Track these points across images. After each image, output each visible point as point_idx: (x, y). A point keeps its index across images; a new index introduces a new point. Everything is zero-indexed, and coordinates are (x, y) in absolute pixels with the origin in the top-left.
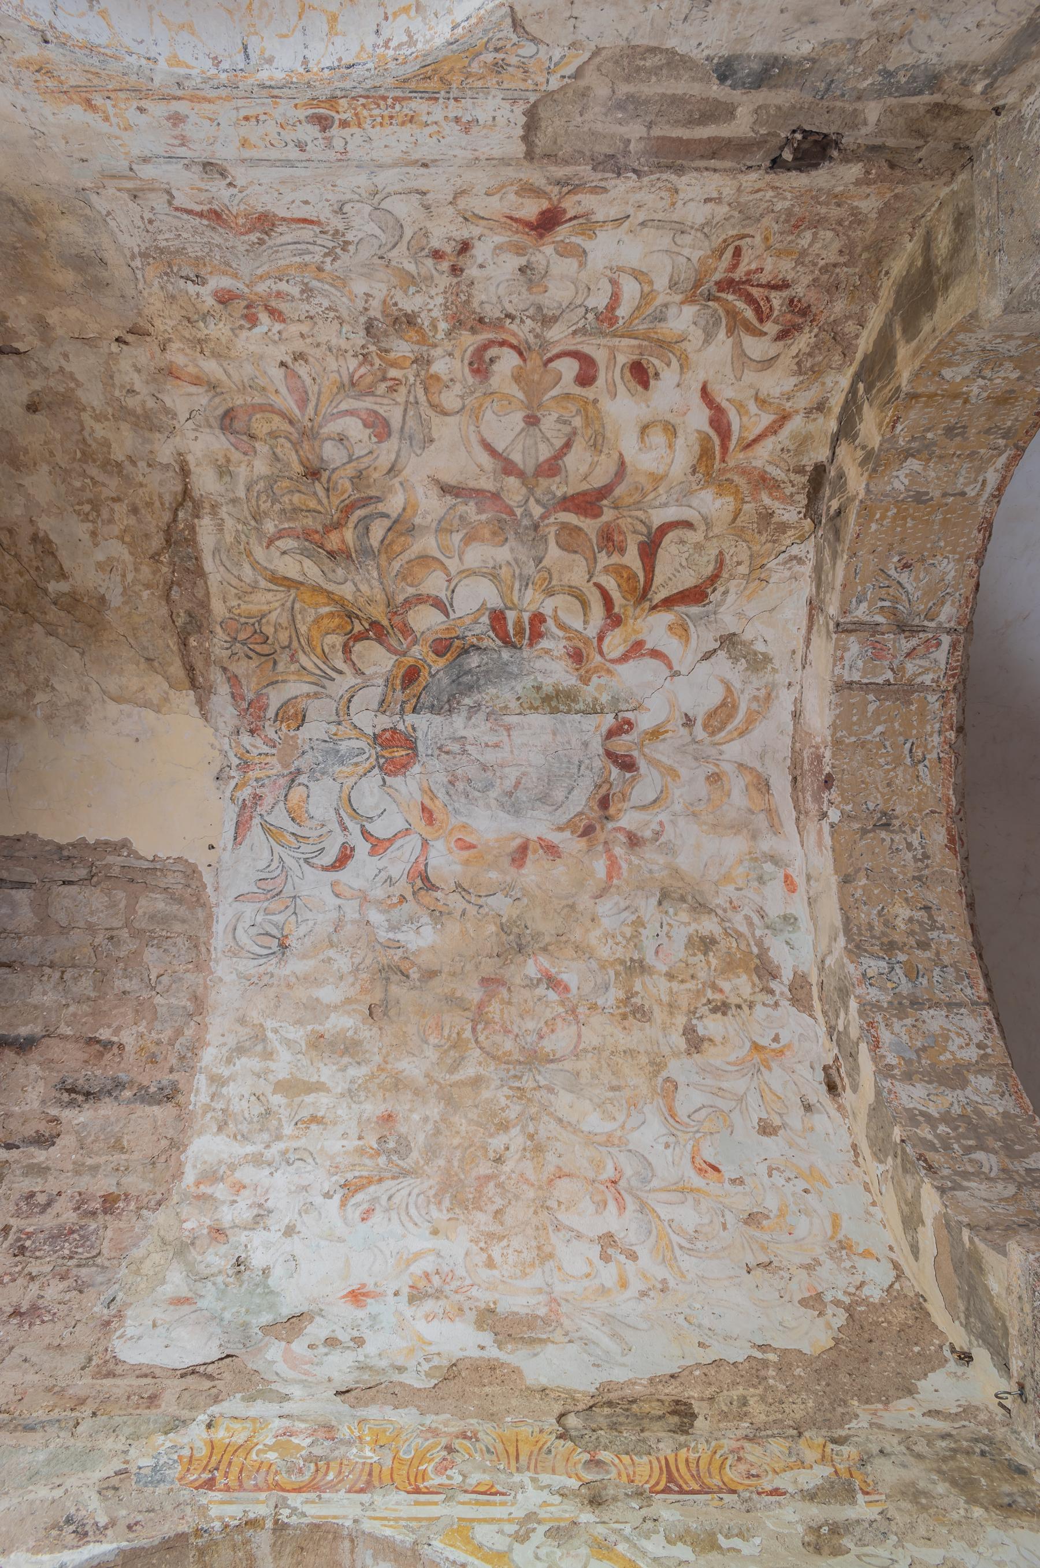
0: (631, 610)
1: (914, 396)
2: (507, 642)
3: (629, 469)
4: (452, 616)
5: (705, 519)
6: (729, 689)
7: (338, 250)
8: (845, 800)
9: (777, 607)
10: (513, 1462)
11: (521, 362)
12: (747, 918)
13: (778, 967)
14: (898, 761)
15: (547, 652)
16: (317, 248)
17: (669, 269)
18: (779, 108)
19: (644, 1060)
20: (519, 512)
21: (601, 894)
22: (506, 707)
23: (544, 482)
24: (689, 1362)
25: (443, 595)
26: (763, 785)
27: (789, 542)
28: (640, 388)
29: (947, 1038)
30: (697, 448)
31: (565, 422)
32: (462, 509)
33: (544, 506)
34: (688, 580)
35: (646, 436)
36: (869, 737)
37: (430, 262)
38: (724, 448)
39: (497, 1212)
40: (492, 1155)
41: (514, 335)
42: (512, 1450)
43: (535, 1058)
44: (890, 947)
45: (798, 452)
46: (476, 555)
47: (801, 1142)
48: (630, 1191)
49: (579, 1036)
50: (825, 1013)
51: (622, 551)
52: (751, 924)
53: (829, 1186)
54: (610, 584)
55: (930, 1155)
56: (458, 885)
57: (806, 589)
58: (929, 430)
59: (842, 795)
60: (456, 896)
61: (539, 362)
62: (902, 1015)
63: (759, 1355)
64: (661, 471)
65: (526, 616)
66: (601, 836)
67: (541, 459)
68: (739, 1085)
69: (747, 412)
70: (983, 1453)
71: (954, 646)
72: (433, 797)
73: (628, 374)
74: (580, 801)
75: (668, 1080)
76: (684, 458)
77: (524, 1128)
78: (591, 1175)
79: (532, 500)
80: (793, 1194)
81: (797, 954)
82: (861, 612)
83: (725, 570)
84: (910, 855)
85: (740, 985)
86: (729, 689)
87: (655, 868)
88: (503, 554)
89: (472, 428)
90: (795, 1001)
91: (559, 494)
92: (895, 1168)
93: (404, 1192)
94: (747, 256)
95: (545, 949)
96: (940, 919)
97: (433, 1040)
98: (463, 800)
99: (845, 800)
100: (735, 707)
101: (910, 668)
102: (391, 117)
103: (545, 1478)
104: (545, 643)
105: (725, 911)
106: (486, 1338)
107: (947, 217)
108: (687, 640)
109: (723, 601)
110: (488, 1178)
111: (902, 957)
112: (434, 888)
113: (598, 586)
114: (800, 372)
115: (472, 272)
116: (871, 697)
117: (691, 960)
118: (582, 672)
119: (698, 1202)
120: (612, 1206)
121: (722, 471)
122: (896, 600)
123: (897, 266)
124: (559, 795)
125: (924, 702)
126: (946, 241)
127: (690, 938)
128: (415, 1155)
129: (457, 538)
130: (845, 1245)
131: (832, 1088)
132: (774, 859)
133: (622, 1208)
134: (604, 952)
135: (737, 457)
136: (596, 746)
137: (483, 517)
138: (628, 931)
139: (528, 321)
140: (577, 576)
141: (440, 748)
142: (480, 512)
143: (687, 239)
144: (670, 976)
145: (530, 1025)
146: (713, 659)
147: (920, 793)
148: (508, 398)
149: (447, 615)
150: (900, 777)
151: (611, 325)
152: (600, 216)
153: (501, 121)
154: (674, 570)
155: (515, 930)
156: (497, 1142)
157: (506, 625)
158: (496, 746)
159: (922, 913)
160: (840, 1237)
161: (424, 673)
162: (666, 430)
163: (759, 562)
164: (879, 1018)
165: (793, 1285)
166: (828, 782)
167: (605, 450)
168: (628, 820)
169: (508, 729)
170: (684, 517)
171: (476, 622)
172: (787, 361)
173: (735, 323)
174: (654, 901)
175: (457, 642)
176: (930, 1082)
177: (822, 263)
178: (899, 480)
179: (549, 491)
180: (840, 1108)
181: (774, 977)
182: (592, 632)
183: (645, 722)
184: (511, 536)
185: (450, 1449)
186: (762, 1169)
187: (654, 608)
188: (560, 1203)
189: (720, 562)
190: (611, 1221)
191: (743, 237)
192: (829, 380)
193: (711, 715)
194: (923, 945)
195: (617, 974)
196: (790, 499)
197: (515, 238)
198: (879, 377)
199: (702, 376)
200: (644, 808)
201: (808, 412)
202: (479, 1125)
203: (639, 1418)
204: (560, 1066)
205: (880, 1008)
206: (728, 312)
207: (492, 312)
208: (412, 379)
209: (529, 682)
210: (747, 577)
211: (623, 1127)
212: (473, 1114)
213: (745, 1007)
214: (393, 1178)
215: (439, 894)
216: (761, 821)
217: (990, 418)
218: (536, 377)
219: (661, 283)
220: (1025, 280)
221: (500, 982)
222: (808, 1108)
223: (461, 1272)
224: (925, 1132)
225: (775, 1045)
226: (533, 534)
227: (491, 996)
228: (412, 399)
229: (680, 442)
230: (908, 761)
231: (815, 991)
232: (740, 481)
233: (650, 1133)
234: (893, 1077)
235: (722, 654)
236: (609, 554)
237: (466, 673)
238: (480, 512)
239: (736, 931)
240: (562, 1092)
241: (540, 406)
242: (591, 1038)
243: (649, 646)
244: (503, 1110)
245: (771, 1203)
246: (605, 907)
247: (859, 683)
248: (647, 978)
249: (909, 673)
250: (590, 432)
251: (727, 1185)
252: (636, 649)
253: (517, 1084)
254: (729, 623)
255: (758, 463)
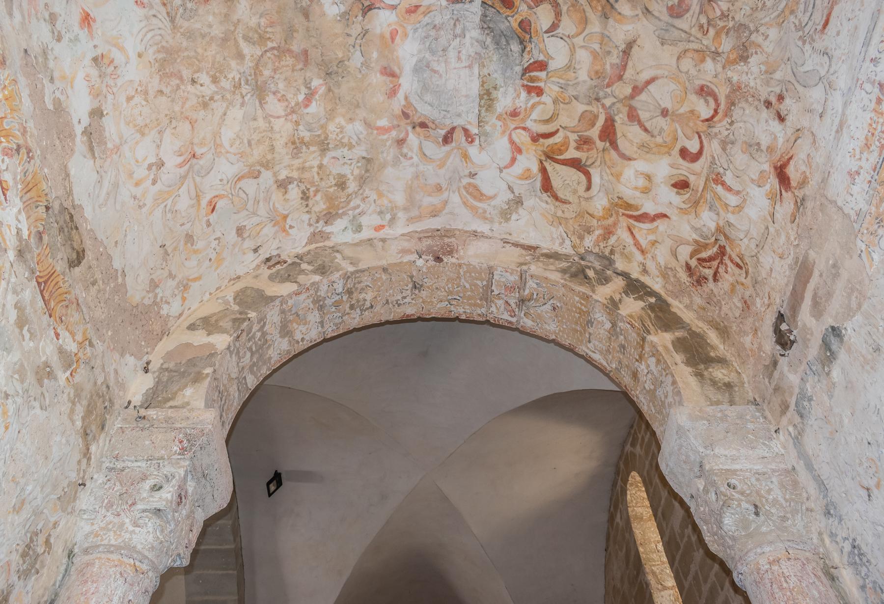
0: (542, 149)
1: (644, 339)
2: (526, 70)
3: (626, 162)
4: (546, 35)
5: (591, 198)
6: (491, 198)
7: (801, 33)
8: (428, 268)
9: (536, 225)
10: (25, 191)
11: (702, 119)
12: (359, 206)
13: (332, 224)
14: (450, 293)
15: (518, 96)
16: (806, 19)
17: (739, 227)
18: (809, 340)
19: (269, 157)
20: (609, 90)
21: (367, 124)
22: (484, 66)
23: (625, 110)
24: (105, 242)
25: (559, 31)
26: (434, 214)
27: (573, 239)
28: (673, 182)
29: (305, 324)
30: (632, 202)
31: (660, 132)
32: (615, 52)
33: (610, 107)
34: (556, 182)
35: (643, 174)
36: (463, 280)
37: (777, 90)
38: (630, 217)
39: (161, 92)
40: (196, 76)
41: (720, 121)
42: (30, 186)
43: (261, 92)
44: (350, 292)
45: (622, 254)
46: (584, 57)
47: (237, 250)
48: (191, 167)
49: (278, 117)
50: (309, 252)
51: (577, 148)
52: (355, 208)
53: (215, 271)
54: (557, 139)
55: (244, 334)
56: (367, 31)
57: (547, 246)
58: (625, 338)
59: (431, 266)
60: (360, 30)
61: (700, 129)
62: (315, 302)
63: (119, 273)
64: (622, 180)
65: (541, 84)
66: (403, 122)
67: (640, 112)
68: (262, 210)
69: (648, 234)
70: (105, 408)
71: (510, 323)
72: (425, 14)
73: (683, 178)
74: (424, 110)
75: (259, 172)
76: (629, 194)
77: (216, 93)
78: (196, 141)
79: (615, 100)
80: (207, 254)
81: (340, 232)
82: (531, 284)
83: (560, 204)
84: (400, 298)
85: (319, 204)
86: (491, 198)
87: (385, 155)
88: (583, 75)
89: (666, 73)
90: (314, 234)
91: (617, 118)
92: (233, 312)
93: (161, 25)
94: (737, 271)
95: (330, 90)
96: (366, 313)
97: (263, 21)
98: (423, 34)
99: (428, 268)
100: (480, 200)
101: (500, 303)
102: (873, 134)
103: (23, 217)
104: (524, 94)
105: (362, 194)
106: (86, 121)
107: (732, 378)
108: (521, 179)
109: (542, 201)
110: (181, 79)
111: (345, 298)
112: (364, 14)
113: (557, 131)
114: (666, 268)
115: (765, 113)
116: (485, 283)
117: (331, 178)
118: (505, 116)
119: (193, 206)
120: (180, 160)
121: (617, 213)
122: (537, 300)
123: (713, 337)
124: (428, 98)
125: (481, 306)
126: (720, 376)
127: (344, 176)
128: (186, 24)
129: (596, 47)
130: (186, 287)
131: (268, 260)
132: (393, 219)
133: (180, 166)
134: (331, 127)
135: (624, 222)
136: (458, 122)
137: (608, 67)
138: (345, 140)
139: (726, 133)
140: (564, 120)
141: (458, 20)
142: (612, 65)
143: (753, 246)
144: (320, 167)
145: (281, 86)
146: (509, 192)
147: (432, 302)
148: (682, 101)
149: (546, 32)
150: (442, 294)
151: (713, 180)
152: (777, 207)
153: (849, 198)
154: (561, 176)
155: (340, 70)
156: (204, 78)
157: (537, 71)
158: (459, 58)
159: (369, 305)
160: (190, 283)
161: (508, 12)
162: (646, 188)
163: (563, 222)
164: (312, 292)
165: (159, 272)
166: (438, 259)
167: (639, 151)
168: (413, 139)
169: (470, 67)
170: (593, 186)
171: (540, 51)
172: (673, 263)
173: (700, 247)
174: (364, 154)
175: (528, 37)
176: (281, 322)
177: (723, 303)
178: (600, 316)
179: (619, 112)
180: (258, 266)
181: (326, 223)
182: (529, 124)
183: (473, 151)
184: (594, 83)
185: (18, 150)
186: (218, 234)
187: (541, 162)
188: (175, 128)
189: (565, 202)
190: (171, 161)
191: (747, 273)
192: (659, 280)
193: (476, 187)
194: (352, 307)
195: (319, 136)
196: (597, 244)
197: (779, 153)
198: (657, 317)
199: (674, 218)
200: (421, 148)
201: (644, 265)
202: (213, 64)
203: (71, 239)
204: (258, 107)
205: (316, 292)
206: (707, 244)
207: (737, 113)
208: (705, 42)
209: (500, 82)
210: (555, 215)
211: (228, 152)
212: (219, 58)
213: (307, 209)
214: (168, 13)
215: (360, 18)
216: (415, 213)
217: (627, 366)
218: (691, 124)
219: (732, 218)
220: (692, 439)
221: (306, 62)
222: (256, 250)
223: (120, 82)
224: (256, 328)
225: (287, 227)
226: (594, 97)
227: (296, 57)
228: (692, 38)
229: (638, 194)
230: (450, 297)
231: (321, 244)
232: (610, 221)
233: (227, 169)
234: (282, 305)
235: (511, 196)
236: (576, 141)
237: (507, 41)
238: (612, 65)
239: (350, 201)
240: (242, 112)
241: (673, 120)
242: (278, 124)
243: (519, 157)
244: (225, 77)
245: (200, 245)
246: (358, 126)
247: (493, 278)
248: (318, 153)
249: (497, 301)
250: (652, 145)
251: (206, 219)
252: (517, 149)
253: (243, 83)
254: (529, 203)
255: (619, 232)
